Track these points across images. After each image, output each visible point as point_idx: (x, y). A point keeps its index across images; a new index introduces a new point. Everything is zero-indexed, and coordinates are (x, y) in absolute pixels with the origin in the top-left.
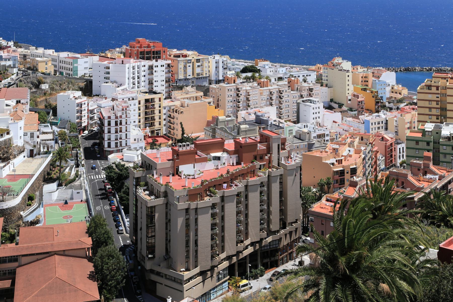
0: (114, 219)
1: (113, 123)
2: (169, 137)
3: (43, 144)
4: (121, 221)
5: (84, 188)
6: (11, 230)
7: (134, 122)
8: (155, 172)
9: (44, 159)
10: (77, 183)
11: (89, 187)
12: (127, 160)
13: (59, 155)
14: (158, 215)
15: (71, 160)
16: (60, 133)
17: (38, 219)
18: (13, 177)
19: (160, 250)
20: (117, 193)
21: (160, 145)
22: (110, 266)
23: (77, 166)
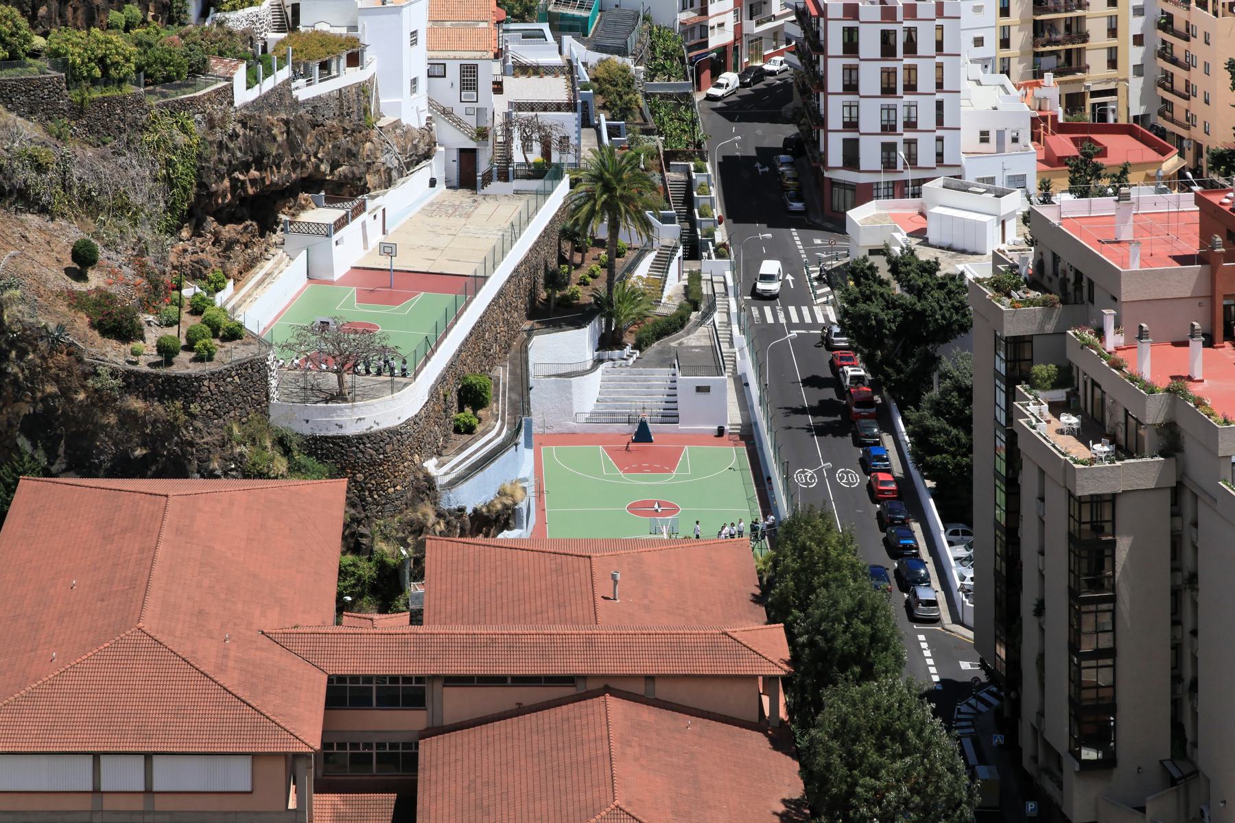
0: (885, 541)
1: (870, 43)
2: (1162, 133)
3: (524, 126)
4: (925, 555)
5: (729, 366)
6: (382, 546)
7: (979, 42)
8: (1109, 315)
9: (533, 204)
10: (695, 339)
11: (759, 367)
12: (946, 241)
13: (608, 188)
14: (1132, 549)
15: (666, 220)
16: (601, 73)
17: (509, 502)
18: (384, 283)
19: (1141, 727)
20: (902, 409)
21: (1121, 177)
22: (888, 789)
23: (694, 251)
